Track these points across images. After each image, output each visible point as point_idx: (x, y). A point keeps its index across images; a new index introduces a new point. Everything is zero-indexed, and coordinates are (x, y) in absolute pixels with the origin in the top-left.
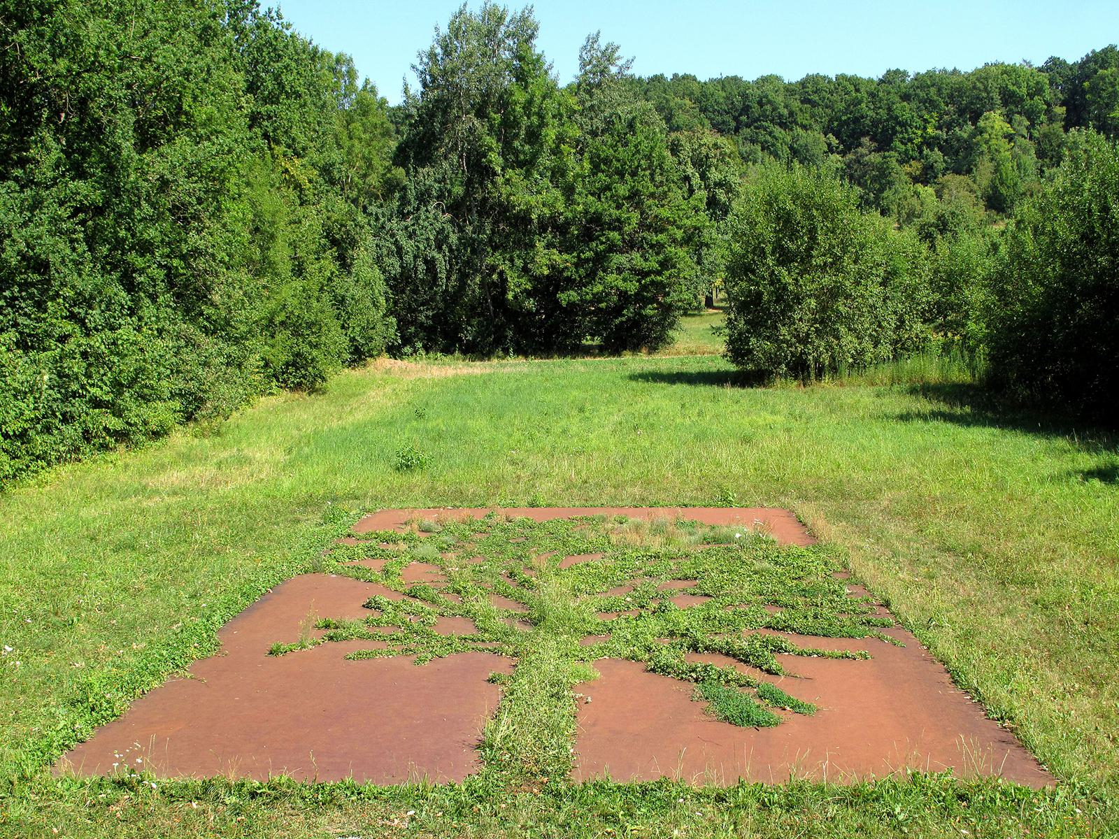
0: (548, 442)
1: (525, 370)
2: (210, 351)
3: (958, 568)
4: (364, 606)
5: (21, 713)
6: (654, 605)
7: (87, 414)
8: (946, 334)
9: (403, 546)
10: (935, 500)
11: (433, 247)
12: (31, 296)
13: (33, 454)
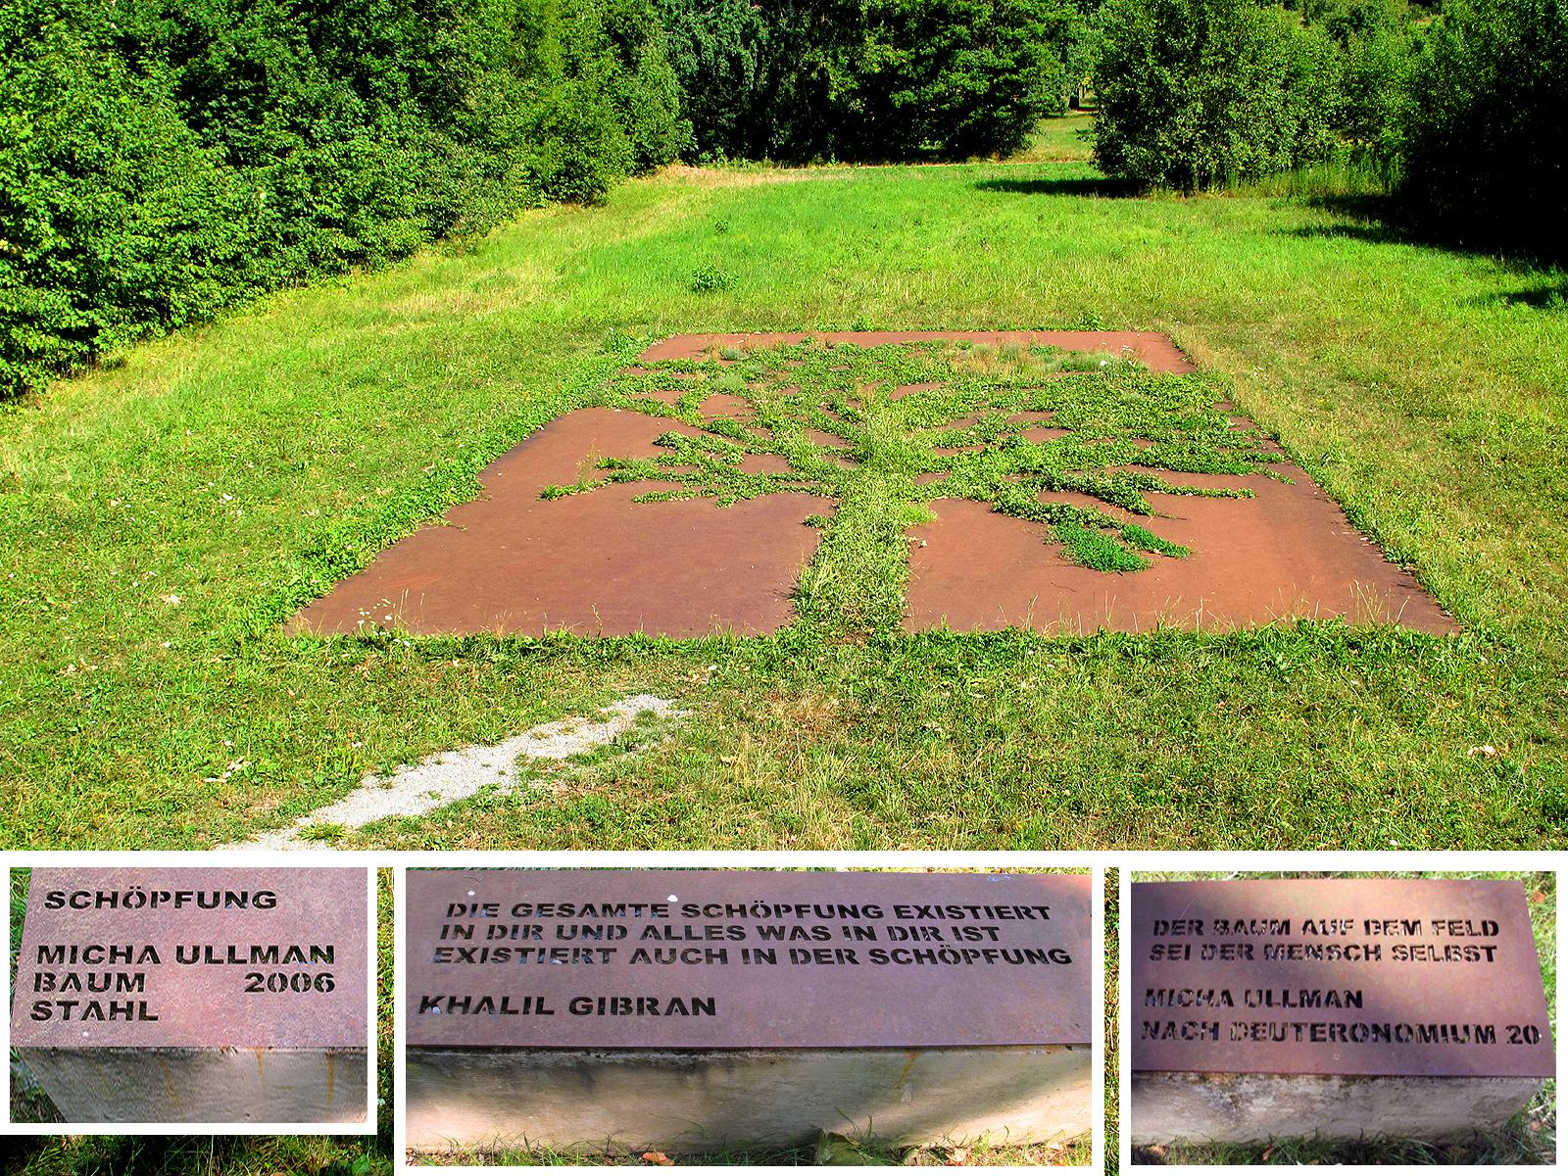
0: (877, 259)
1: (850, 177)
2: (464, 161)
3: (1358, 398)
4: (654, 443)
5: (246, 567)
6: (1001, 439)
7: (314, 234)
8: (1356, 141)
9: (702, 376)
10: (1336, 324)
11: (739, 42)
12: (243, 106)
13: (248, 280)
